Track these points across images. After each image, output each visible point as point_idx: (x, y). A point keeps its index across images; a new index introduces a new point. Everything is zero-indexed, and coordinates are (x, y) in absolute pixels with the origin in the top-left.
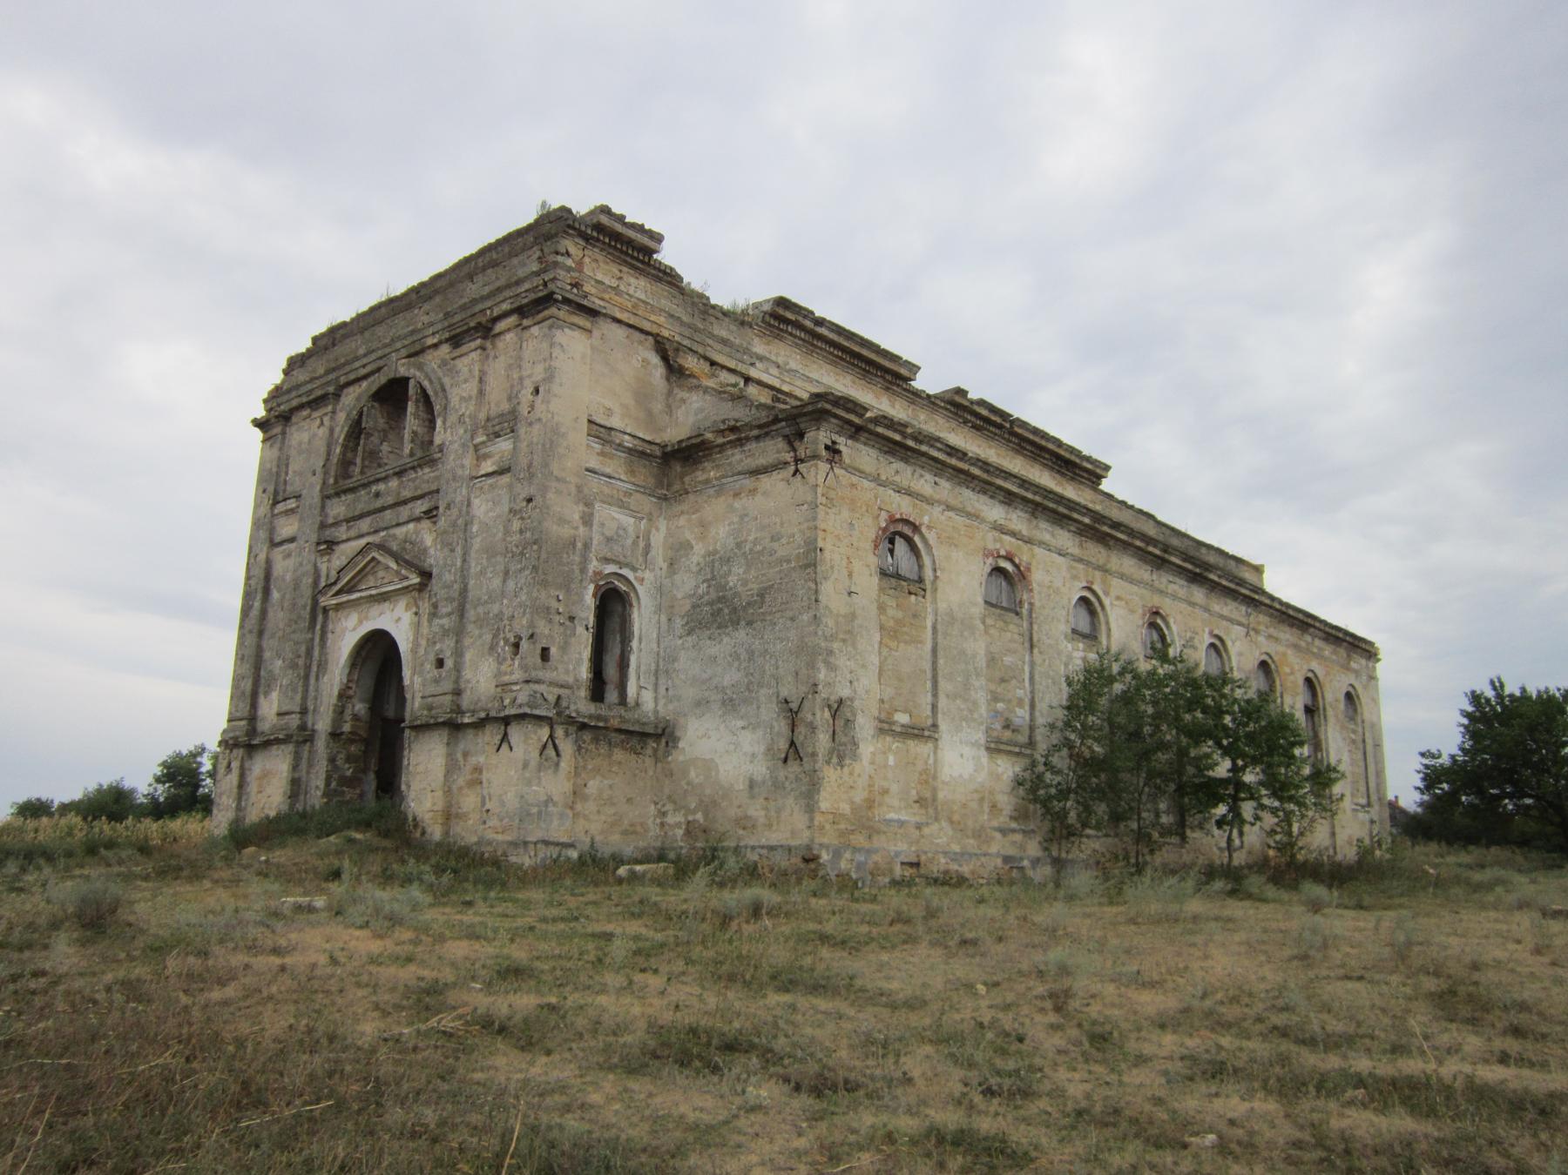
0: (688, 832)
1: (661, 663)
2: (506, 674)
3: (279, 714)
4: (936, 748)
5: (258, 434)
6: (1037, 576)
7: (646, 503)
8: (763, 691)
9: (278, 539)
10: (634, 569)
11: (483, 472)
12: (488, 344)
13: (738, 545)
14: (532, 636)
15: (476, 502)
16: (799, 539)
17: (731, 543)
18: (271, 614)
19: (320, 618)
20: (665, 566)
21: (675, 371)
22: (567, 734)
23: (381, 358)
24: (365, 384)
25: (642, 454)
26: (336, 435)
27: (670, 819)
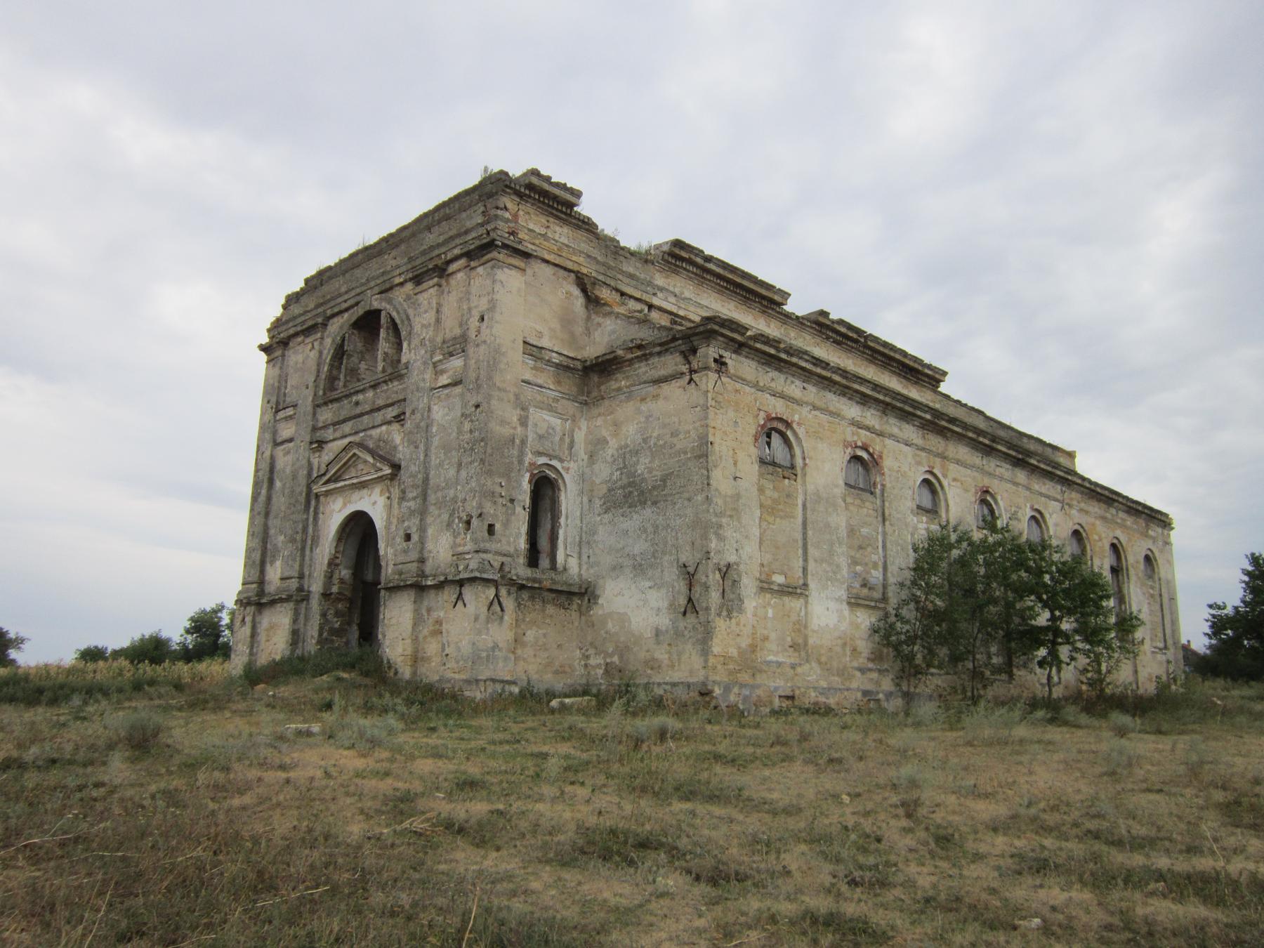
0: (607, 672)
1: (584, 535)
2: (460, 545)
3: (282, 579)
4: (807, 603)
5: (263, 357)
6: (888, 463)
7: (571, 407)
8: (666, 558)
9: (279, 440)
10: (561, 461)
11: (440, 384)
12: (443, 282)
13: (645, 440)
14: (480, 515)
15: (435, 408)
16: (693, 434)
17: (639, 439)
18: (274, 500)
19: (313, 503)
20: (586, 457)
21: (592, 301)
22: (509, 593)
23: (358, 294)
24: (346, 315)
25: (567, 368)
26: (324, 357)
27: (592, 662)
